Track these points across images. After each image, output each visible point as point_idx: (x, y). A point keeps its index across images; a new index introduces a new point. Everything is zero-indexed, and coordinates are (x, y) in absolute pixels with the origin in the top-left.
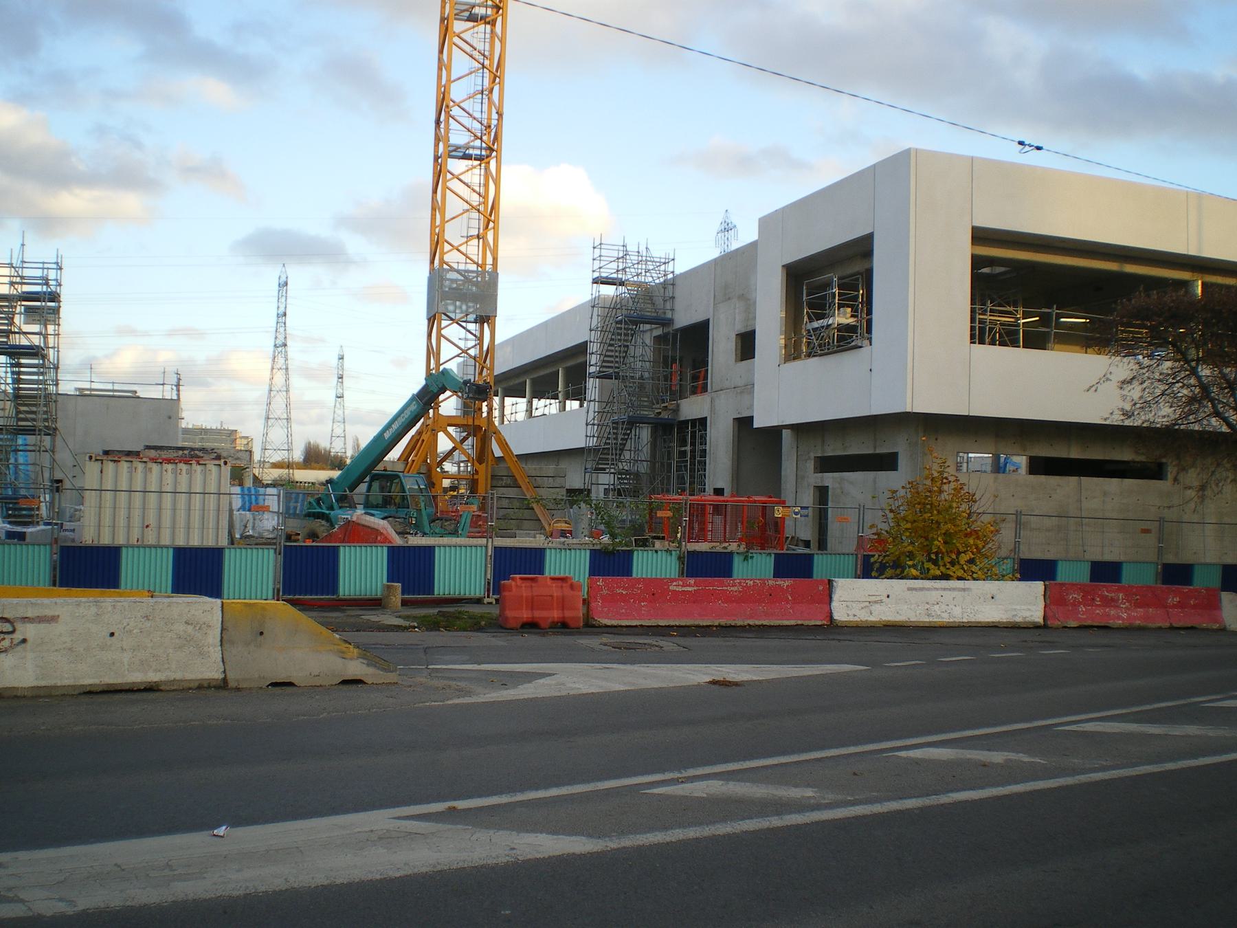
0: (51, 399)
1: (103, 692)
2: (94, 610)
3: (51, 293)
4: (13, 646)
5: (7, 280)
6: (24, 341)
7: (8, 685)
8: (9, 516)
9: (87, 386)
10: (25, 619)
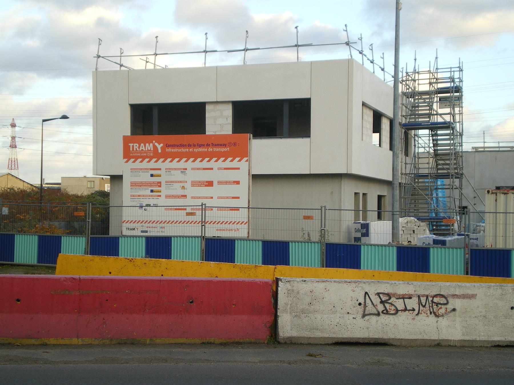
0: (458, 155)
1: (507, 346)
2: (499, 291)
3: (456, 87)
4: (447, 312)
5: (428, 81)
6: (440, 120)
7: (444, 338)
8: (433, 230)
9: (482, 145)
10: (454, 296)
